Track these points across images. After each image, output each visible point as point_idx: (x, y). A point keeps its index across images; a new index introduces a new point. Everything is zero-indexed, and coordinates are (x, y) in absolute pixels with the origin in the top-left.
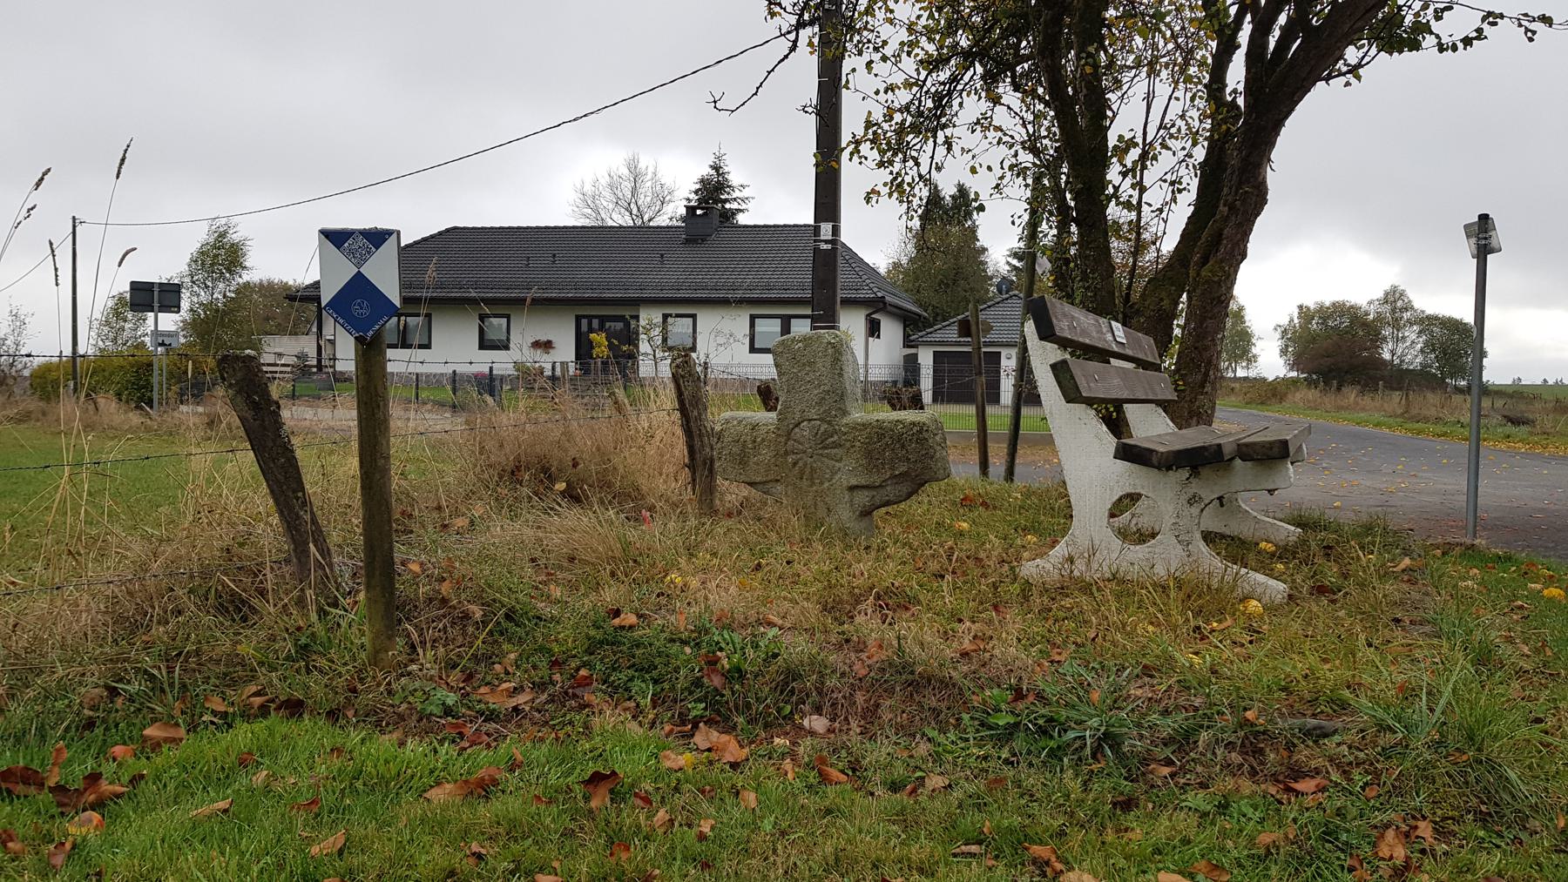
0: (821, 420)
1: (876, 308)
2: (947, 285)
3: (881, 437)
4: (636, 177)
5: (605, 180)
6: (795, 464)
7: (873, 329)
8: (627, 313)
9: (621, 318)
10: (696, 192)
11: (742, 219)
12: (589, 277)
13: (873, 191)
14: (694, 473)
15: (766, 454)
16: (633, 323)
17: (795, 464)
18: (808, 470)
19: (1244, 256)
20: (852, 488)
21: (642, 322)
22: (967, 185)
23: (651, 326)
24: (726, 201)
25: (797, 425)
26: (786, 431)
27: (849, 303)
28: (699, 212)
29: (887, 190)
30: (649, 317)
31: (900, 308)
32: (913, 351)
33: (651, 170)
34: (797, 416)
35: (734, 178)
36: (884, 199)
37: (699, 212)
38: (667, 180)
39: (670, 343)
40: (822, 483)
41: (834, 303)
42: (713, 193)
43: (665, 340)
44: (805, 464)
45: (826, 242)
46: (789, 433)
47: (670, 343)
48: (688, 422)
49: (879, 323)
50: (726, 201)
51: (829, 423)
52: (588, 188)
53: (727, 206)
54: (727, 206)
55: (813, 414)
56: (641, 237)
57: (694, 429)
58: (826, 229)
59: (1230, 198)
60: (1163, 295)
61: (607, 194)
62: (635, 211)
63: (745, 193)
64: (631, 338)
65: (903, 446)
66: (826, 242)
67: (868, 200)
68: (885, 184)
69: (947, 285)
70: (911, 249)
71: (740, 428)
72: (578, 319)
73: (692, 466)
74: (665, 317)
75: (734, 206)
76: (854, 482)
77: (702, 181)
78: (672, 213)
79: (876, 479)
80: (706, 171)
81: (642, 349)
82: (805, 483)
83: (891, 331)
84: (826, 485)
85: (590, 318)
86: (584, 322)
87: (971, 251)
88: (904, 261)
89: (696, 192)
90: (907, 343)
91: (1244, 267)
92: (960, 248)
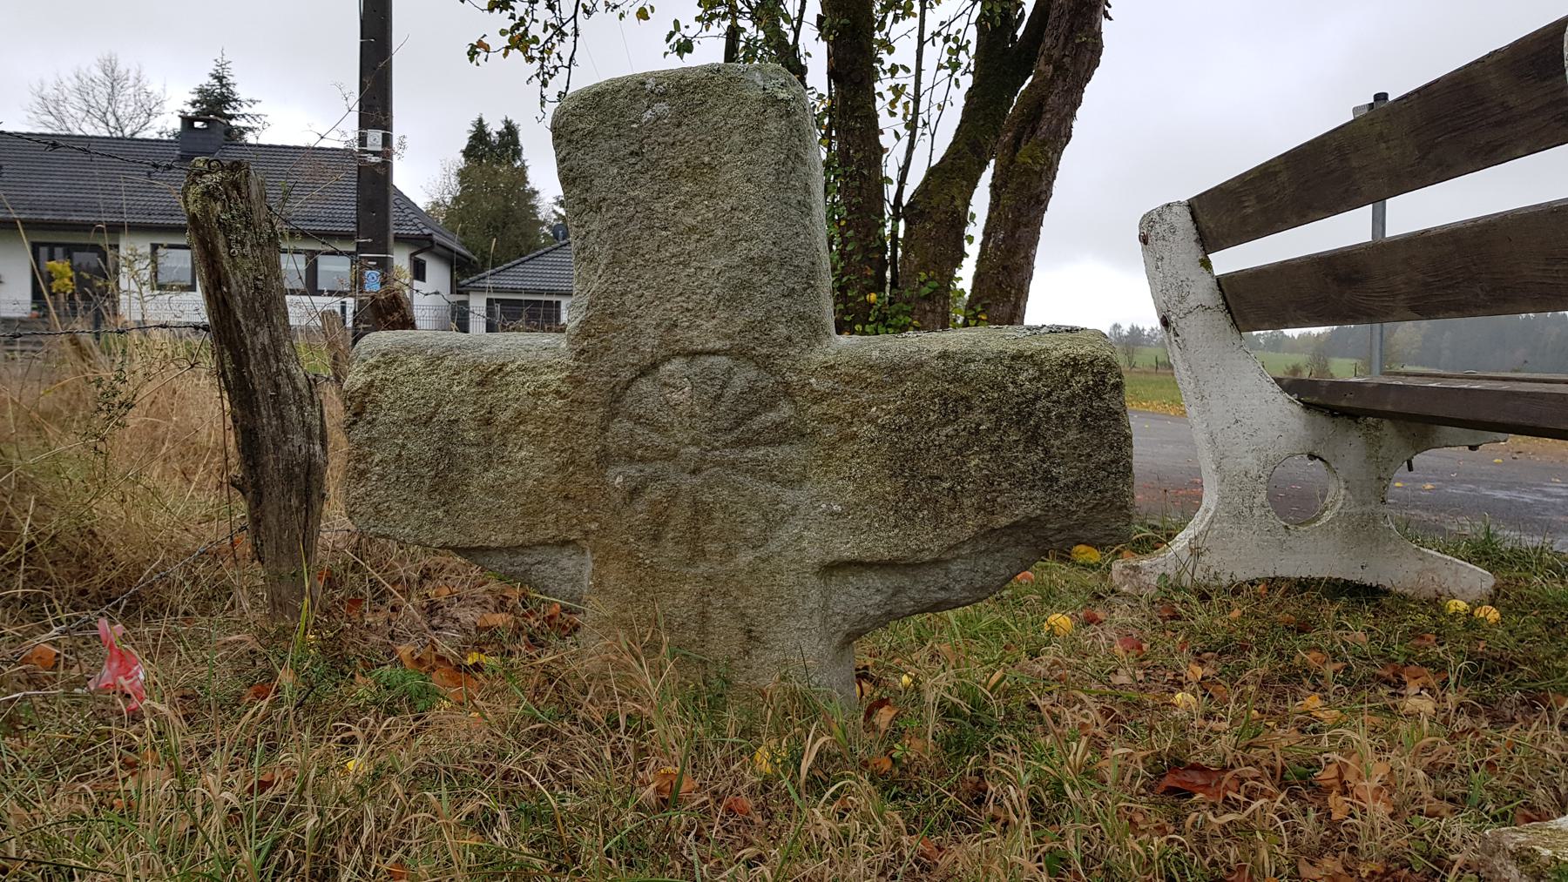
0: (740, 354)
1: (422, 245)
2: (496, 228)
3: (954, 405)
4: (114, 82)
5: (70, 84)
6: (634, 493)
7: (419, 272)
8: (104, 241)
9: (95, 248)
10: (193, 104)
11: (250, 138)
12: (52, 195)
13: (480, 44)
14: (257, 502)
15: (528, 462)
16: (110, 253)
17: (634, 493)
18: (680, 515)
19: (1069, 137)
20: (833, 568)
21: (123, 252)
22: (515, 122)
23: (137, 257)
24: (232, 117)
25: (648, 370)
26: (608, 385)
27: (401, 240)
28: (198, 124)
29: (505, 41)
30: (132, 247)
31: (451, 250)
32: (462, 297)
33: (132, 75)
34: (649, 344)
35: (241, 91)
36: (496, 57)
37: (198, 124)
38: (154, 87)
39: (162, 279)
40: (729, 553)
41: (386, 239)
42: (214, 106)
43: (155, 273)
44: (673, 496)
45: (375, 153)
46: (614, 401)
47: (162, 279)
48: (240, 360)
49: (424, 265)
50: (232, 117)
51: (765, 363)
52: (49, 91)
53: (233, 123)
54: (233, 123)
55: (707, 333)
56: (122, 153)
57: (259, 383)
58: (375, 137)
59: (1056, 54)
60: (955, 191)
61: (74, 98)
62: (112, 122)
63: (255, 109)
64: (107, 272)
65: (1033, 439)
66: (375, 153)
67: (472, 54)
68: (503, 32)
69: (496, 228)
70: (455, 186)
71: (438, 381)
72: (35, 248)
73: (252, 484)
74: (155, 247)
75: (242, 123)
76: (846, 549)
77: (200, 91)
78: (166, 124)
79: (925, 540)
80: (206, 80)
81: (123, 284)
82: (670, 550)
83: (438, 275)
84: (745, 558)
85: (52, 246)
86: (44, 251)
87: (519, 192)
88: (448, 199)
89: (193, 104)
90: (456, 288)
91: (1068, 153)
92: (510, 190)
